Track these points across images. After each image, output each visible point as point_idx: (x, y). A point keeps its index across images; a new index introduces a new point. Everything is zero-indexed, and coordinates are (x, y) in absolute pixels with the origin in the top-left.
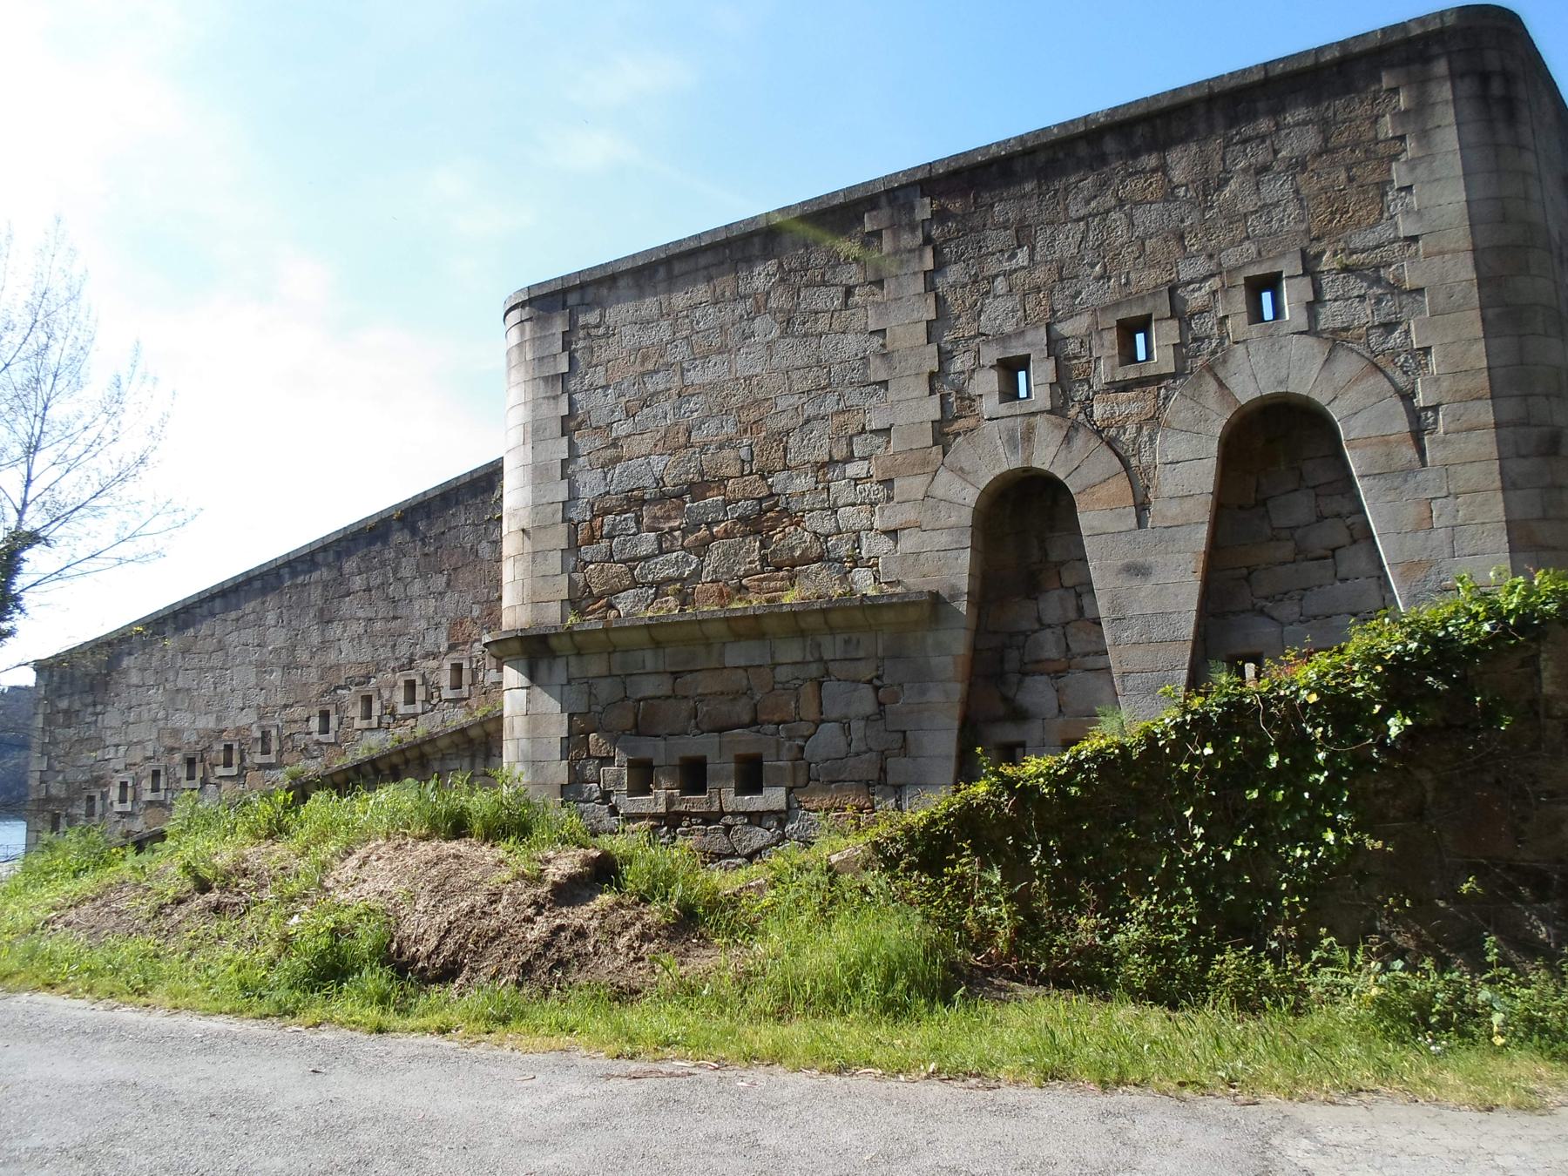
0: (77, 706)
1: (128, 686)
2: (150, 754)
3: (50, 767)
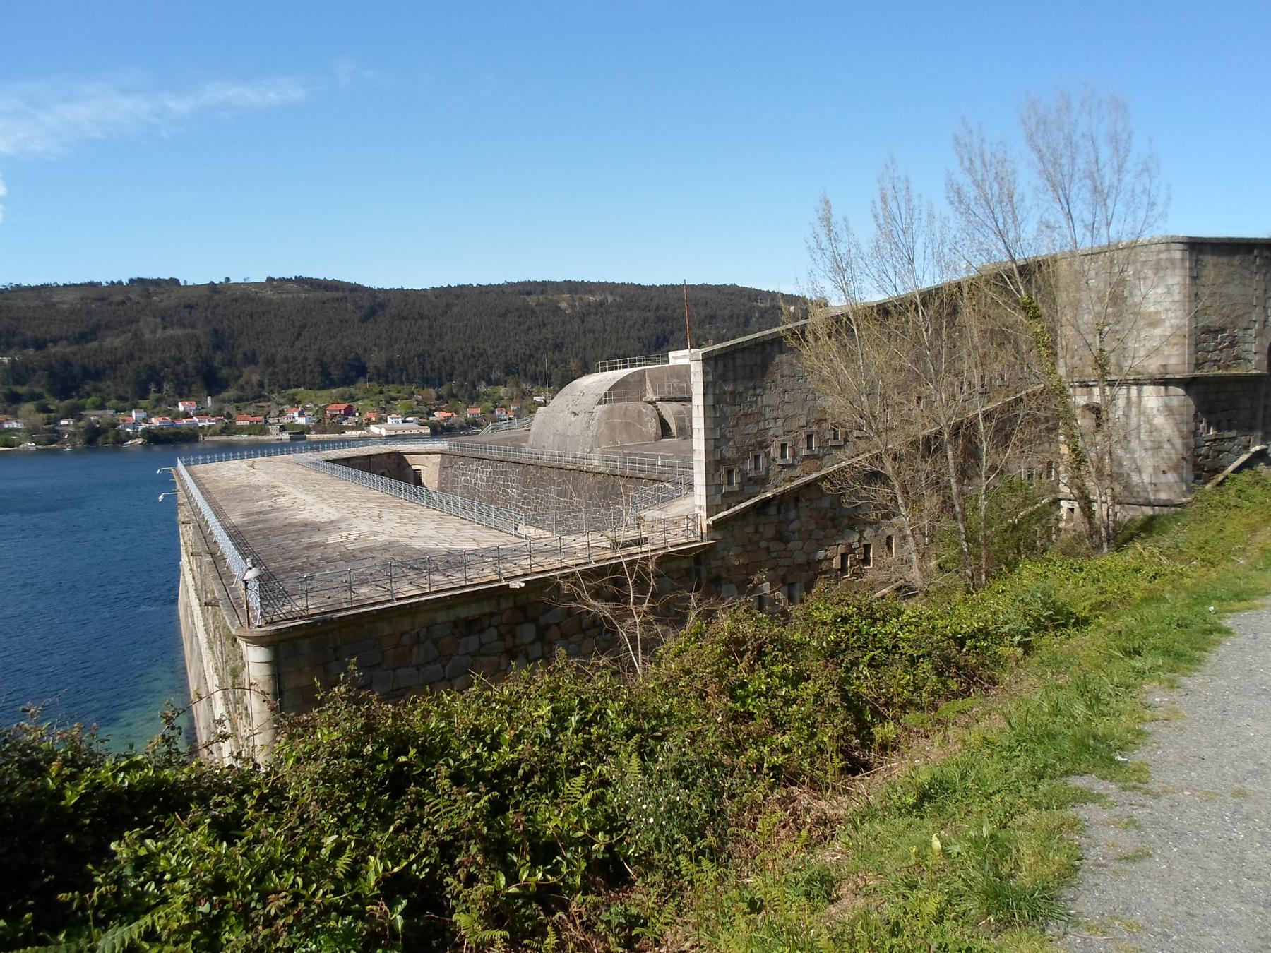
1: (782, 376)
2: (804, 423)
3: (723, 436)
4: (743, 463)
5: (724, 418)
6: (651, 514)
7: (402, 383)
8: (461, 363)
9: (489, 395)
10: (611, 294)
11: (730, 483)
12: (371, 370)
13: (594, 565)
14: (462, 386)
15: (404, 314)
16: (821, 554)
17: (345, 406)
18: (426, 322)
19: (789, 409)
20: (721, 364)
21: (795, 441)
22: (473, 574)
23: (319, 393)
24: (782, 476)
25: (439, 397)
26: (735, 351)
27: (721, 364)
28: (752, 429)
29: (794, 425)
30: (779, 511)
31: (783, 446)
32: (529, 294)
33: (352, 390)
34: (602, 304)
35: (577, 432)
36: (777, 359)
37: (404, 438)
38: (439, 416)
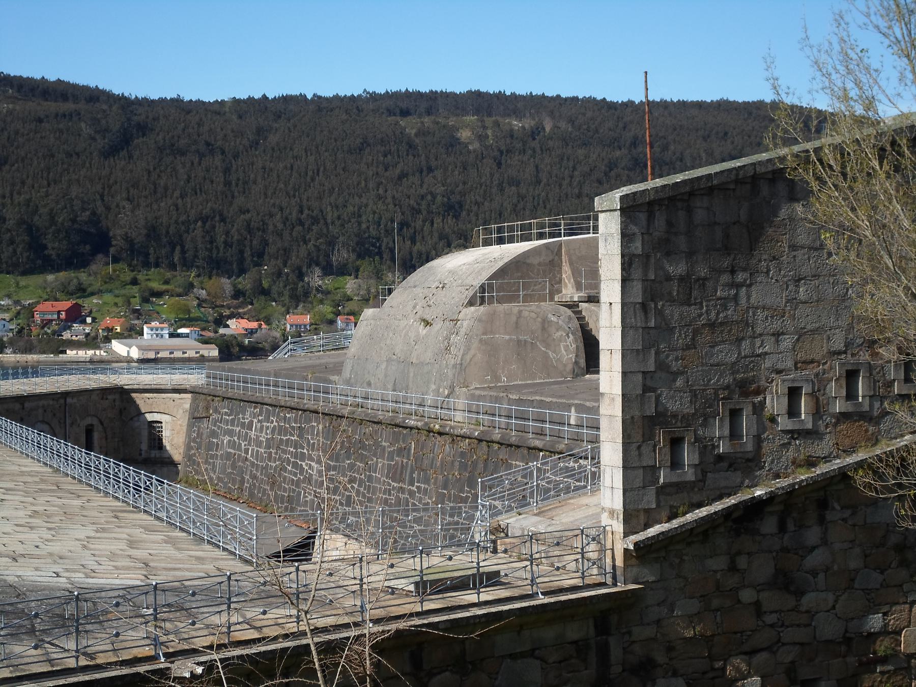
0: (702, 271)
1: (793, 247)
2: (839, 345)
3: (662, 366)
4: (705, 424)
5: (665, 329)
6: (519, 523)
7: (172, 267)
8: (280, 235)
9: (327, 293)
10: (552, 114)
11: (675, 464)
12: (118, 242)
13: (543, 600)
14: (279, 274)
15: (183, 142)
16: (875, 622)
17: (66, 304)
18: (218, 160)
19: (807, 317)
20: (660, 222)
21: (819, 384)
22: (100, 645)
23: (23, 281)
24: (791, 453)
25: (238, 294)
26: (691, 194)
27: (660, 222)
28: (726, 354)
29: (818, 349)
30: (782, 528)
31: (794, 393)
32: (405, 113)
33: (83, 276)
34: (535, 132)
35: (428, 356)
36: (783, 213)
37: (172, 363)
38: (235, 327)
